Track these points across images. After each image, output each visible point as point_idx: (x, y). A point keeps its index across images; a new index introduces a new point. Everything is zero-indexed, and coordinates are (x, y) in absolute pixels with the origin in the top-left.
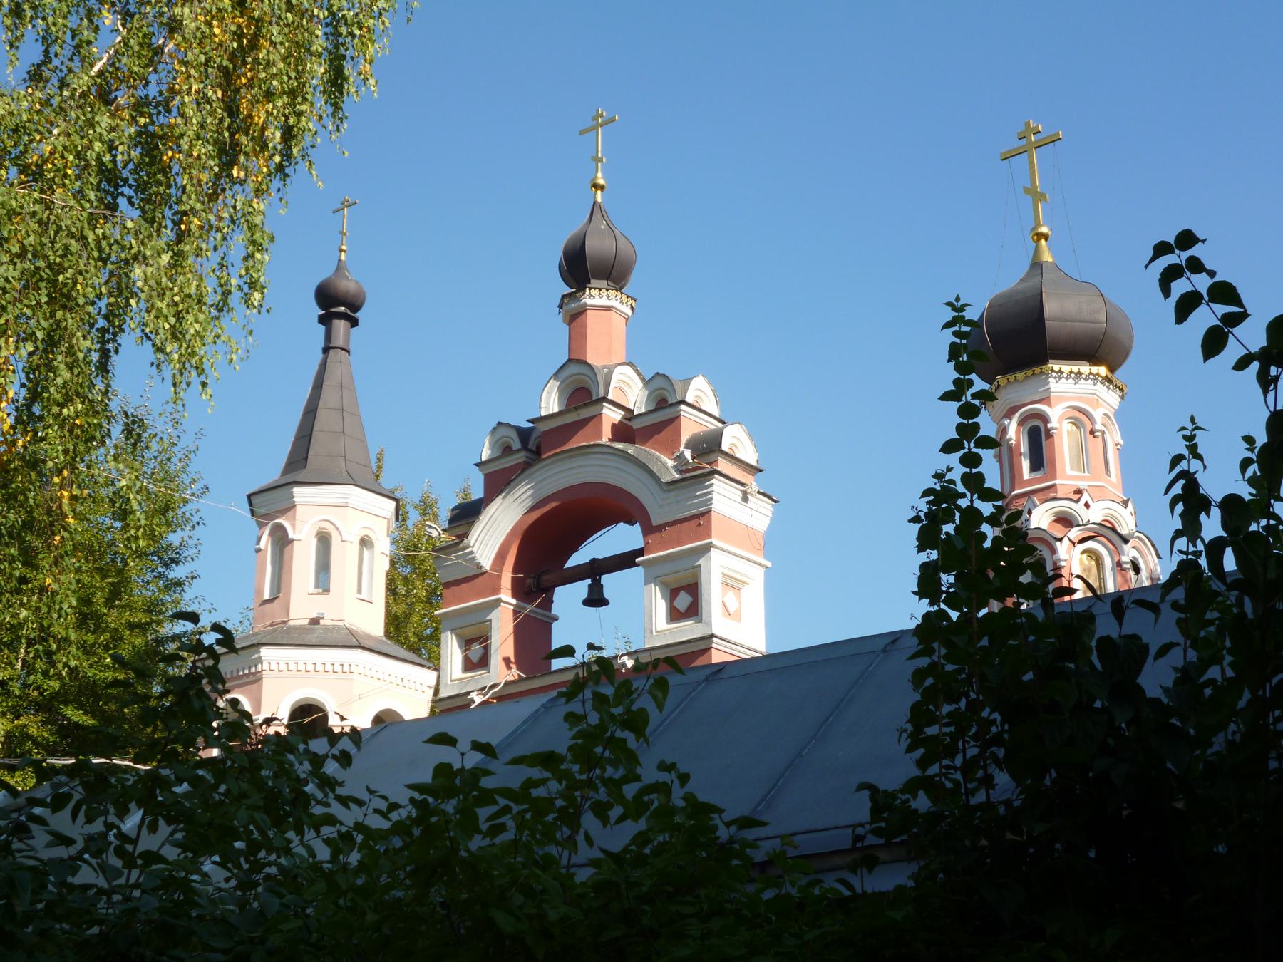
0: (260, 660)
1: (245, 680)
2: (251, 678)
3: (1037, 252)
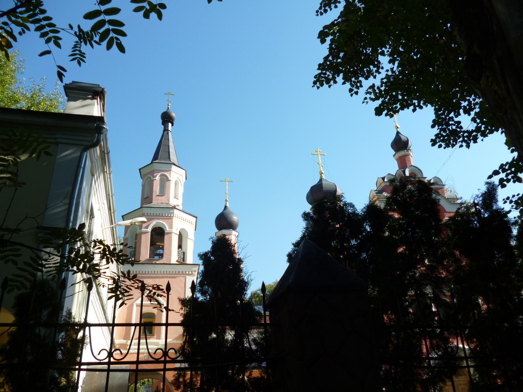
0: (173, 213)
1: (165, 217)
2: (168, 218)
3: (226, 204)
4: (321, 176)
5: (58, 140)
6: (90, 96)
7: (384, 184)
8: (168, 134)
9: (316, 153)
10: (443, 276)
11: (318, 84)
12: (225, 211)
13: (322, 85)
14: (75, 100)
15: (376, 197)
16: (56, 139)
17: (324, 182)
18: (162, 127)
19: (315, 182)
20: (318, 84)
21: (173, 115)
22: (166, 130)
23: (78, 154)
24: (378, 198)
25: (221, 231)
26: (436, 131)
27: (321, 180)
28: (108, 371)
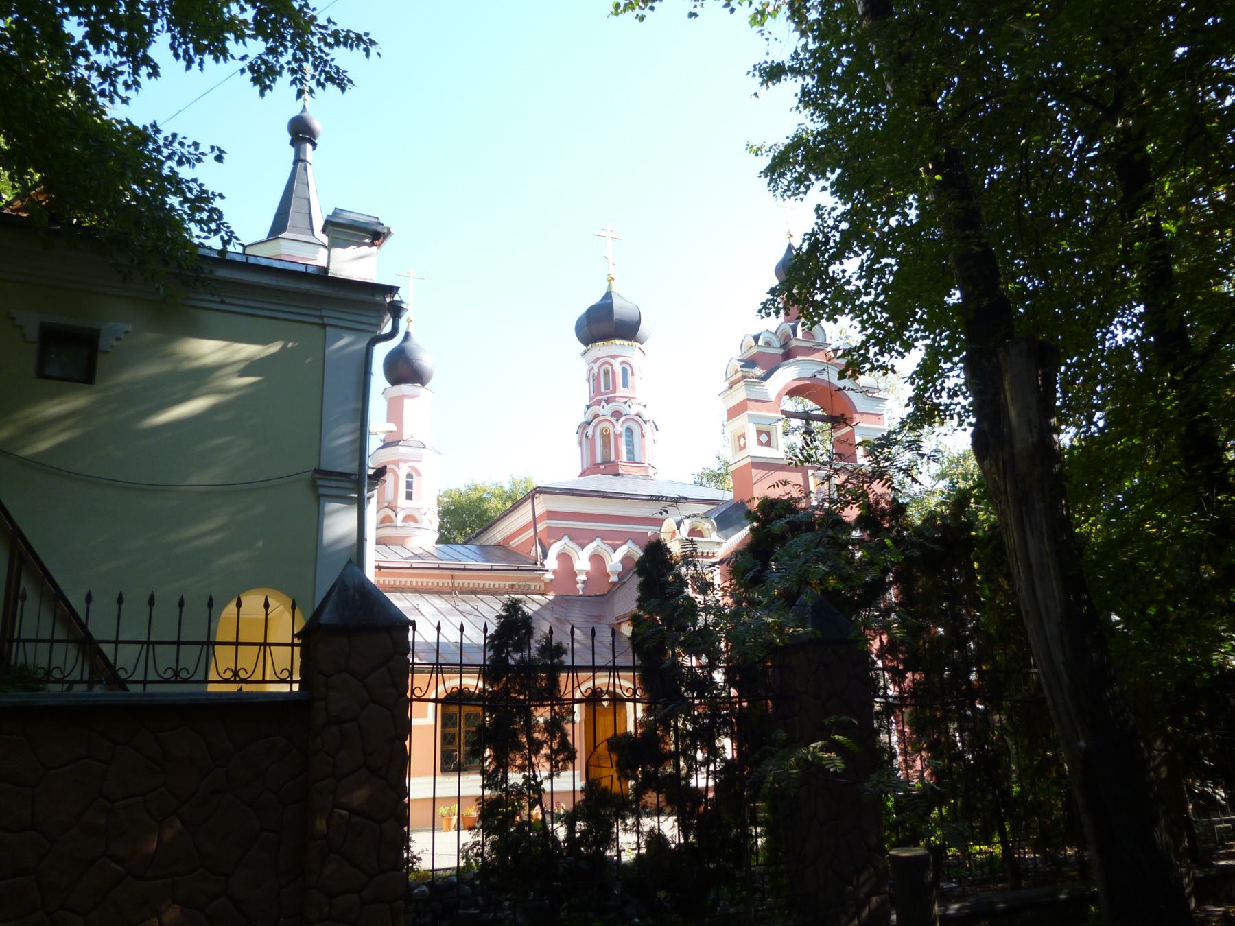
4: (610, 286)
5: (326, 321)
6: (367, 241)
7: (755, 350)
8: (305, 169)
9: (603, 233)
10: (1003, 718)
11: (763, 314)
12: (407, 344)
13: (768, 315)
14: (344, 245)
15: (740, 374)
16: (322, 317)
17: (615, 300)
18: (291, 151)
19: (596, 298)
20: (763, 314)
21: (317, 124)
22: (299, 160)
23: (362, 345)
24: (744, 377)
25: (397, 387)
26: (911, 409)
27: (608, 295)
28: (461, 665)
